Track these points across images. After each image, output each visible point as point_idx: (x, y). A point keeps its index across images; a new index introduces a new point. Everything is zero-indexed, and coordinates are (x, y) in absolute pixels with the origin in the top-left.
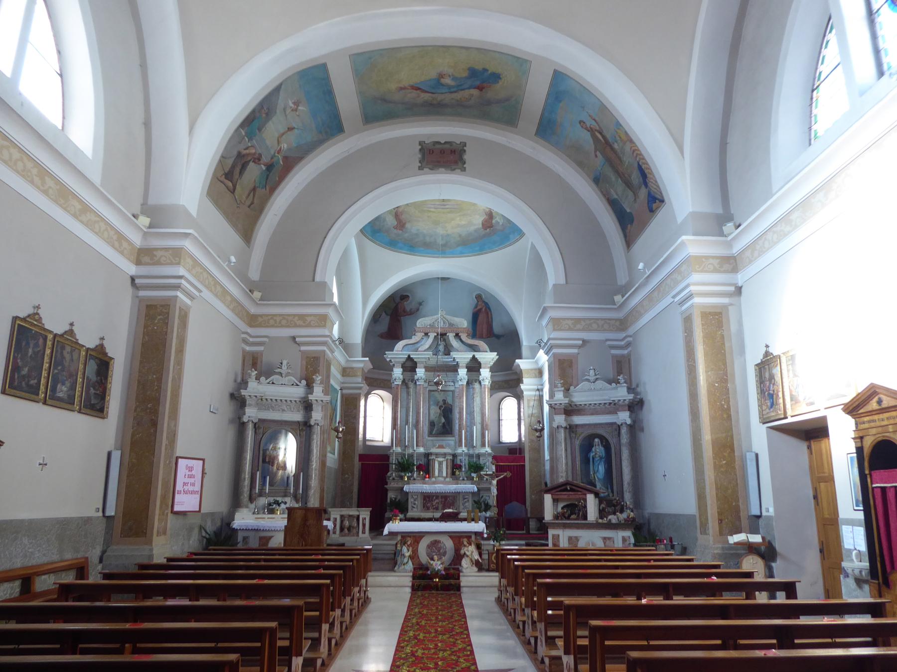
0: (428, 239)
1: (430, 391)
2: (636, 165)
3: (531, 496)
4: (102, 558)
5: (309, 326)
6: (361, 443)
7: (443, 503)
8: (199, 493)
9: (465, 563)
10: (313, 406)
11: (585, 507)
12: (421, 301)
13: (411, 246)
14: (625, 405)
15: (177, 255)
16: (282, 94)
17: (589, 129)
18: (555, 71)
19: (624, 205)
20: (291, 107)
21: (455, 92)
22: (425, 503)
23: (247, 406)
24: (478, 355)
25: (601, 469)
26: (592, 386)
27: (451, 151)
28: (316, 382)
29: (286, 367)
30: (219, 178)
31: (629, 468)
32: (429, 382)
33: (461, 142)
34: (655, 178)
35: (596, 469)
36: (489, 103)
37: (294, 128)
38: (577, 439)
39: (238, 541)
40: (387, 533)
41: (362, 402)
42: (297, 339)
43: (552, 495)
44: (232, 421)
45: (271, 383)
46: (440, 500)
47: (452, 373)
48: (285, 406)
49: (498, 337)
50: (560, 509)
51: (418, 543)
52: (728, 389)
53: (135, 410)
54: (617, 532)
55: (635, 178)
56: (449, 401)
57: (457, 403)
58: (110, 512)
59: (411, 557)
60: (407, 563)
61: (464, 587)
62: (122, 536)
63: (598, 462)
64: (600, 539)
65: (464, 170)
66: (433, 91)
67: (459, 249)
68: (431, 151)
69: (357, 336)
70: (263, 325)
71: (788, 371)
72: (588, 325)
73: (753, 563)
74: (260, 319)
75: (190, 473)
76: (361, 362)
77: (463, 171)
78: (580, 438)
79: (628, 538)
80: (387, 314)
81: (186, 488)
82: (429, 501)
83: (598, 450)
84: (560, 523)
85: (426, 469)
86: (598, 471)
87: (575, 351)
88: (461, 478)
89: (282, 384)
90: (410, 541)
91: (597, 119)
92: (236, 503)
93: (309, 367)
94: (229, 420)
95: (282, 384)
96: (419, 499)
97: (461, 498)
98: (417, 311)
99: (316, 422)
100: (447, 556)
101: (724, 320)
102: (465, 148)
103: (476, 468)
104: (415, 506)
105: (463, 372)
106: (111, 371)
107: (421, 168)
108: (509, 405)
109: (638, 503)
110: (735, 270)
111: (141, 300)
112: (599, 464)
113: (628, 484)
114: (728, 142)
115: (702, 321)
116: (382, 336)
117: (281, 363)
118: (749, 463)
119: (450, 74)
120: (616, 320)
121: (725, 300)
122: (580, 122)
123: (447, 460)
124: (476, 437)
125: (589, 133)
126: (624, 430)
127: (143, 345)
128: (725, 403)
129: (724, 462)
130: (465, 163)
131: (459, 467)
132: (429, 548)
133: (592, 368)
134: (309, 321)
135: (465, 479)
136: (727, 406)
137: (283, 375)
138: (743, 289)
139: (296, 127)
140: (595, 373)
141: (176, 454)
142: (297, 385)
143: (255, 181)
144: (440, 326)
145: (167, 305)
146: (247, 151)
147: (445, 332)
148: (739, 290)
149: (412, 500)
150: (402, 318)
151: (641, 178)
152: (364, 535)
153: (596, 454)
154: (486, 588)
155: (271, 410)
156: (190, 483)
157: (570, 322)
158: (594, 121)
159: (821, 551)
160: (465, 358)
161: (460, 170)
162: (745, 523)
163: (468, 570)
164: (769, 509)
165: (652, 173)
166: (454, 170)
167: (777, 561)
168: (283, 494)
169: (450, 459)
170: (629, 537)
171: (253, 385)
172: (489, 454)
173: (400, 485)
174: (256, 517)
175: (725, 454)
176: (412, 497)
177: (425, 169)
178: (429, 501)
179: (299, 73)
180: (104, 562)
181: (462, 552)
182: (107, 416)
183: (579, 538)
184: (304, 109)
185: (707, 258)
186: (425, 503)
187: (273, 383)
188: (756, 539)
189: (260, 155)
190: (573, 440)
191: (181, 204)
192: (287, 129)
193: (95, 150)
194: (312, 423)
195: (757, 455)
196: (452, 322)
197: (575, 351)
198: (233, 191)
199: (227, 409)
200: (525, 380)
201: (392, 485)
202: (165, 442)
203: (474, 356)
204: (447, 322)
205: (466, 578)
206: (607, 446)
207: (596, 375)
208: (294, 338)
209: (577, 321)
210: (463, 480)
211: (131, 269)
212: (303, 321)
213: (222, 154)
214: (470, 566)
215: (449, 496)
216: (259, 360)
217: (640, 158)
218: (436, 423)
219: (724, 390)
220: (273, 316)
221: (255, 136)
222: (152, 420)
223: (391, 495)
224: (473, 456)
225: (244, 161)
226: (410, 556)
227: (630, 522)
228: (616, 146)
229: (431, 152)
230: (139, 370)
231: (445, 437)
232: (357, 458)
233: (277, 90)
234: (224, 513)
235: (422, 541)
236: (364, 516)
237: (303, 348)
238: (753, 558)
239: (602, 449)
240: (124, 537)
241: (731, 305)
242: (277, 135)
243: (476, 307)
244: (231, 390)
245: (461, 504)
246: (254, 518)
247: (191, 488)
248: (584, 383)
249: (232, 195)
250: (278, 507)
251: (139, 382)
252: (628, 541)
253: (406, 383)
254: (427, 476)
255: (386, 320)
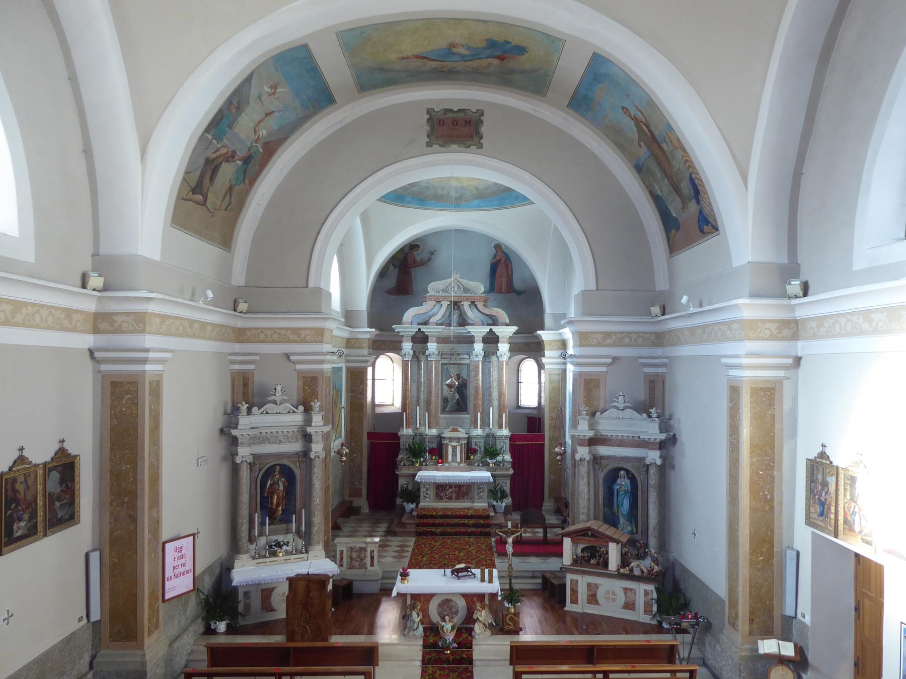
0: (439, 192)
1: (443, 364)
2: (688, 176)
3: (550, 477)
4: (92, 664)
5: (304, 341)
6: (369, 411)
7: (457, 492)
8: (192, 571)
9: (478, 628)
10: (313, 437)
11: (607, 553)
12: (433, 250)
13: (421, 200)
14: (656, 443)
15: (140, 322)
16: (254, 82)
17: (633, 117)
18: (595, 54)
19: (669, 207)
20: (267, 92)
21: (470, 60)
22: (438, 492)
23: (239, 445)
24: (496, 329)
25: (626, 504)
26: (621, 414)
27: (466, 122)
28: (315, 409)
29: (280, 393)
30: (185, 197)
31: (656, 511)
32: (442, 354)
33: (477, 110)
34: (710, 201)
35: (620, 504)
36: (512, 72)
37: (274, 111)
38: (601, 471)
39: (239, 600)
40: (396, 594)
41: (370, 370)
42: (292, 358)
43: (572, 538)
44: (224, 459)
45: (264, 412)
46: (454, 489)
47: (467, 345)
48: (281, 437)
49: (519, 293)
50: (579, 551)
51: (429, 602)
52: (774, 477)
53: (111, 505)
54: (640, 585)
55: (685, 186)
56: (464, 375)
57: (472, 379)
58: (96, 616)
59: (422, 622)
60: (417, 628)
61: (474, 645)
62: (111, 640)
63: (623, 496)
64: (621, 590)
65: (480, 146)
66: (443, 59)
67: (476, 202)
68: (442, 122)
69: (362, 302)
70: (253, 340)
71: (845, 489)
72: (621, 339)
73: (782, 674)
74: (249, 333)
75: (180, 554)
76: (366, 332)
77: (479, 148)
78: (605, 471)
79: (650, 592)
80: (395, 267)
81: (176, 571)
82: (442, 490)
83: (623, 482)
84: (579, 570)
85: (438, 453)
86: (622, 505)
87: (604, 369)
88: (476, 464)
89: (277, 413)
90: (420, 606)
91: (643, 111)
92: (235, 548)
93: (306, 387)
94: (221, 457)
95: (277, 413)
96: (432, 489)
97: (476, 488)
98: (428, 262)
99: (317, 455)
100: (459, 616)
101: (777, 397)
102: (482, 118)
103: (491, 452)
104: (427, 496)
105: (479, 347)
106: (77, 476)
107: (429, 145)
108: (529, 366)
109: (663, 546)
110: (795, 336)
111: (104, 376)
112: (624, 498)
113: (654, 528)
114: (803, 172)
115: (751, 398)
116: (390, 292)
117: (275, 389)
118: (788, 561)
119: (464, 44)
120: (651, 333)
121: (781, 373)
122: (623, 108)
123: (461, 444)
124: (493, 419)
125: (633, 122)
126: (652, 471)
127: (111, 429)
128: (768, 492)
129: (761, 558)
130: (481, 138)
131: (475, 451)
132: (440, 607)
133: (621, 394)
134: (304, 335)
135: (481, 465)
136: (771, 497)
137: (278, 403)
138: (802, 362)
139: (275, 110)
140: (625, 400)
141: (161, 539)
142: (294, 412)
143: (230, 180)
144: (453, 294)
145: (135, 382)
146: (218, 153)
147: (460, 300)
148: (798, 360)
149: (424, 490)
150: (412, 269)
151: (692, 191)
152: (372, 568)
153: (620, 488)
154: (500, 662)
155: (266, 442)
156: (180, 565)
157: (599, 337)
158: (639, 112)
159: (856, 665)
160: (481, 332)
161: (475, 147)
162: (777, 623)
163: (481, 636)
164: (805, 612)
165: (706, 192)
166: (469, 146)
167: (807, 671)
168: (284, 532)
169: (465, 444)
170: (652, 591)
171: (244, 421)
172: (506, 437)
173: (411, 472)
174: (257, 562)
175: (763, 549)
176: (425, 487)
177: (434, 146)
178: (442, 490)
179: (273, 57)
180: (95, 669)
181: (475, 617)
182: (79, 521)
183: (599, 585)
184: (284, 90)
185: (764, 321)
186: (438, 492)
187: (267, 413)
188: (788, 650)
189: (234, 152)
190: (597, 472)
191: (139, 254)
192: (264, 115)
193: (21, 222)
194: (312, 456)
195: (798, 554)
196: (467, 287)
197: (604, 369)
198: (204, 203)
199: (219, 447)
200: (547, 353)
201: (403, 471)
202: (147, 536)
203: (491, 330)
204: (461, 286)
205: (479, 646)
206: (633, 480)
207: (625, 402)
208: (287, 356)
209: (607, 335)
210: (479, 465)
211: (88, 340)
212: (298, 335)
213: (187, 168)
214: (483, 630)
215: (463, 486)
216: (250, 380)
217: (692, 171)
218: (449, 400)
219: (769, 478)
220: (263, 330)
221: (225, 135)
222: (131, 515)
223: (402, 482)
224: (490, 436)
225: (214, 166)
226: (421, 621)
227: (653, 576)
228: (664, 146)
229: (441, 122)
230: (110, 458)
231: (459, 414)
232: (365, 436)
233: (249, 79)
234: (223, 557)
235: (432, 600)
236: (372, 549)
237: (299, 367)
238: (782, 670)
239: (628, 481)
240: (113, 641)
241: (787, 378)
242: (252, 125)
243: (495, 257)
244: (220, 426)
245: (476, 494)
246: (255, 563)
247: (181, 570)
248: (611, 409)
249: (204, 207)
250: (280, 550)
251: (111, 472)
252: (650, 595)
253: (417, 356)
254: (440, 461)
255: (394, 273)
